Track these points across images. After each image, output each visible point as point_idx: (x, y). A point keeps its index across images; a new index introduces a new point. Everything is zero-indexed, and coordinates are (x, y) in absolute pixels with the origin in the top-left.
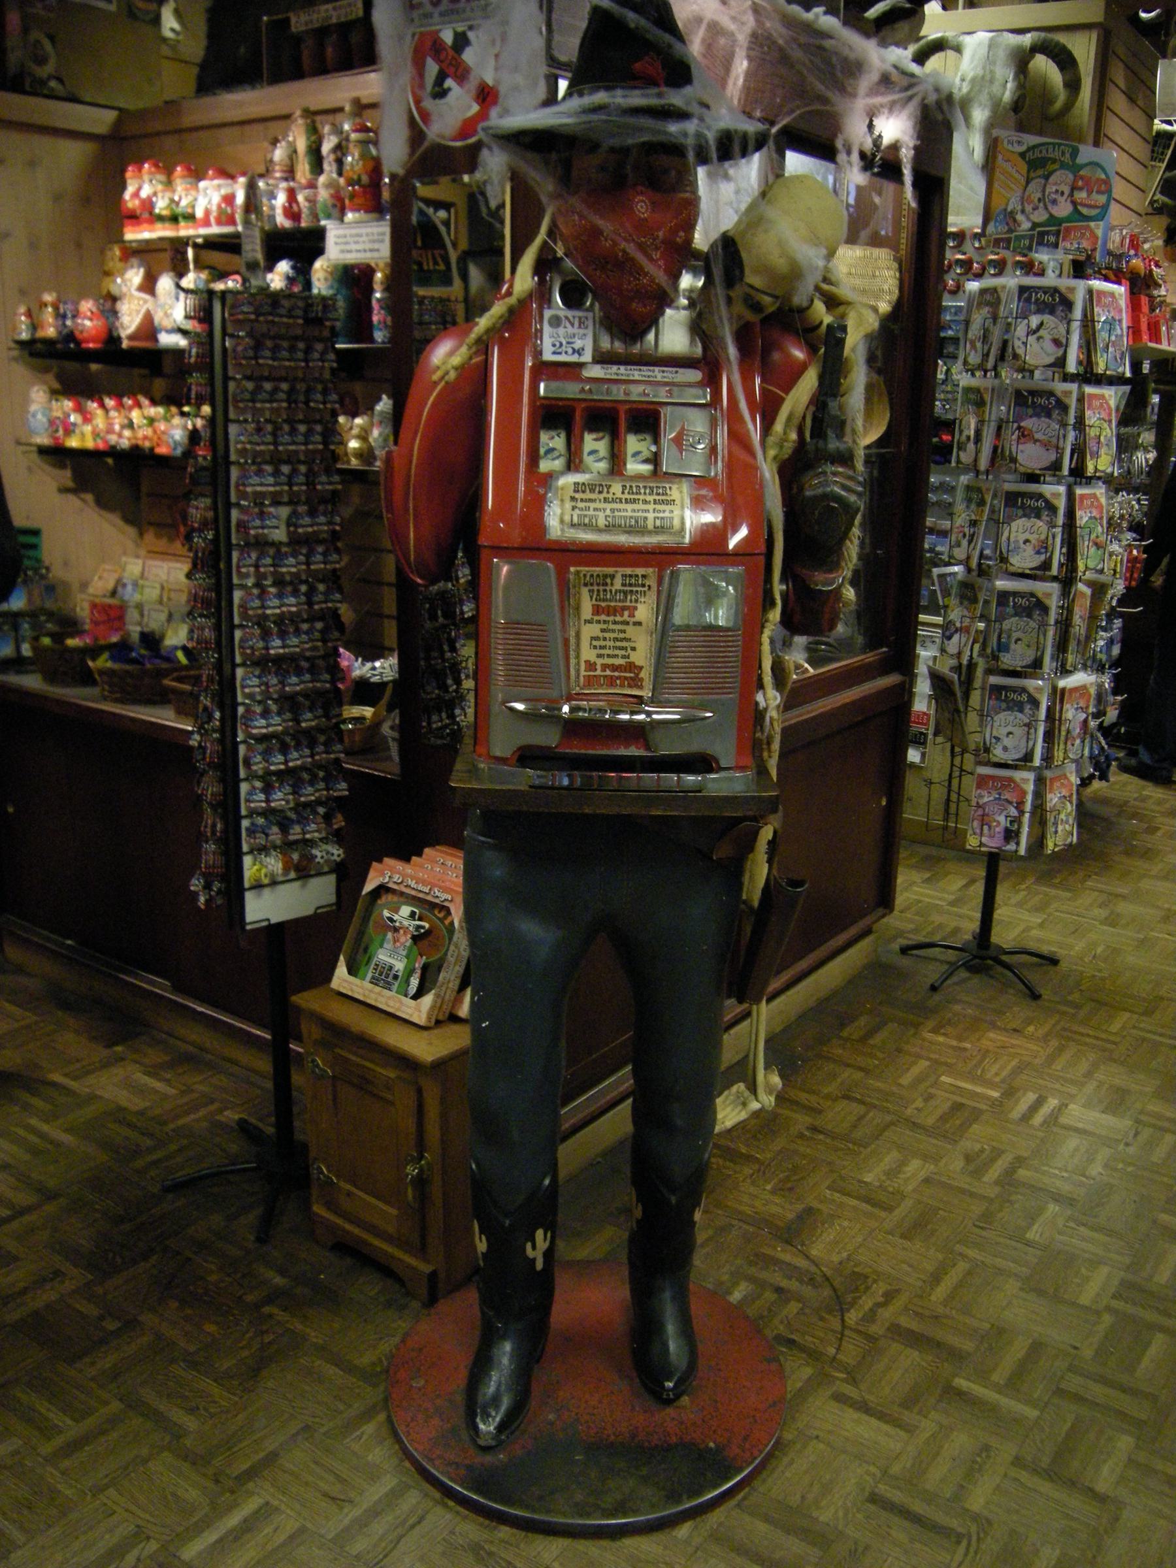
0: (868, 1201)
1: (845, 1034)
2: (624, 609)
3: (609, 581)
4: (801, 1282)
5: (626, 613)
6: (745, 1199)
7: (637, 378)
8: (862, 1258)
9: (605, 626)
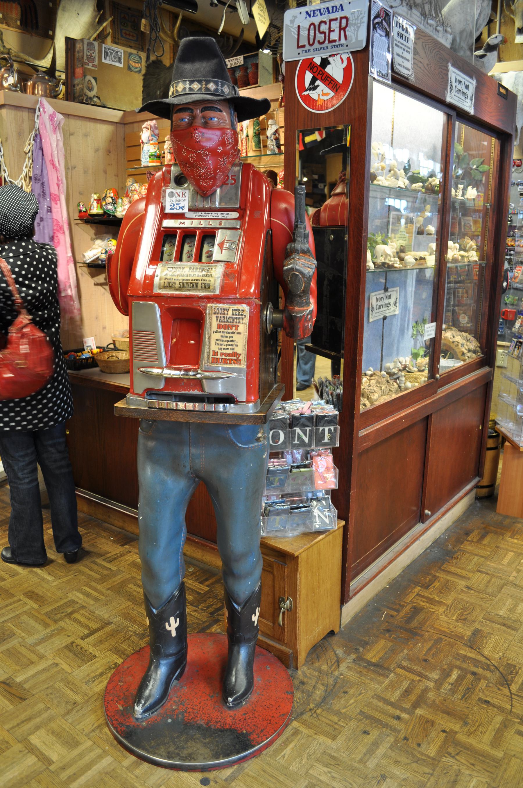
0: (504, 625)
1: (469, 538)
2: (233, 326)
3: (226, 312)
4: (484, 669)
5: (234, 328)
6: (444, 624)
7: (210, 217)
8: (510, 656)
9: (223, 334)
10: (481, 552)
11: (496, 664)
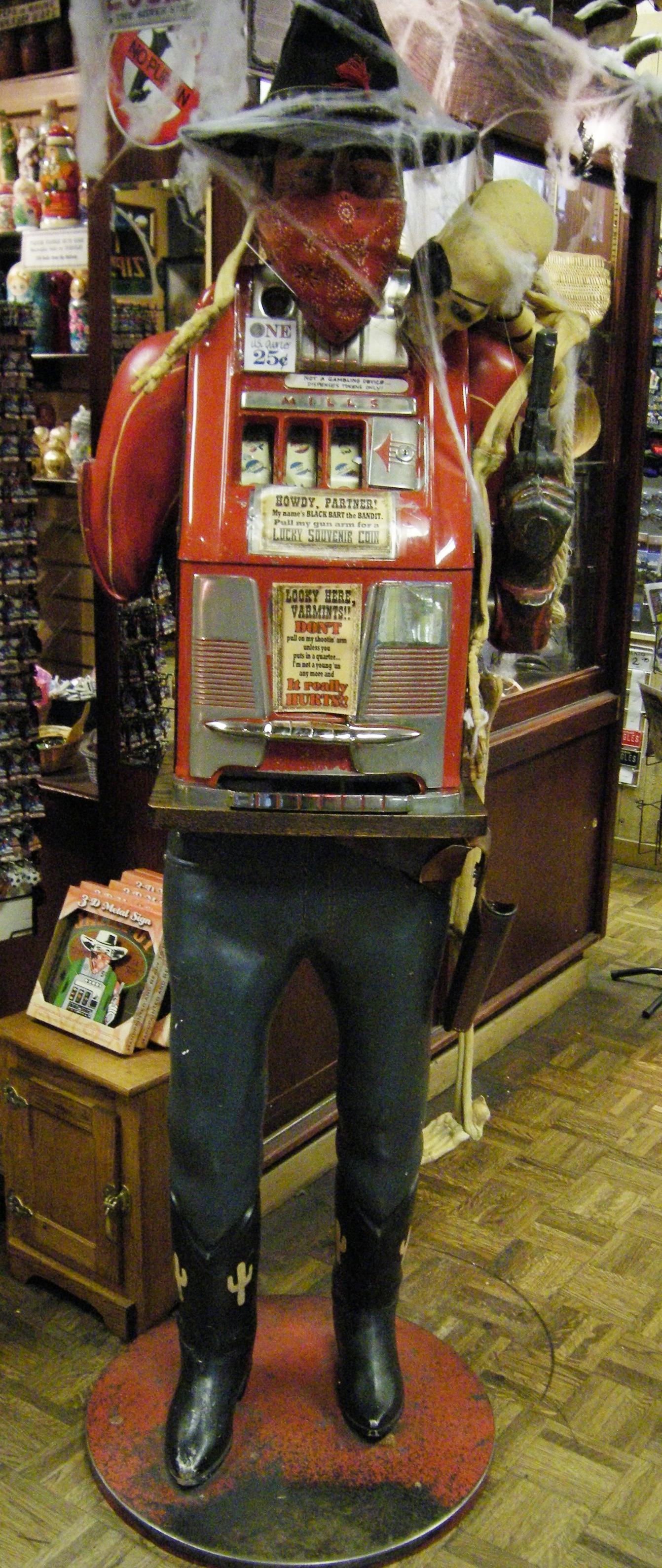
0: (579, 1233)
1: (555, 1062)
2: (328, 625)
3: (312, 596)
4: (510, 1317)
5: (330, 630)
7: (341, 388)
8: (572, 1293)
9: (308, 643)
10: (571, 1090)
11: (538, 1308)
